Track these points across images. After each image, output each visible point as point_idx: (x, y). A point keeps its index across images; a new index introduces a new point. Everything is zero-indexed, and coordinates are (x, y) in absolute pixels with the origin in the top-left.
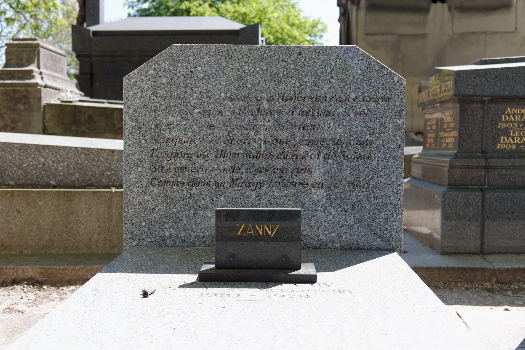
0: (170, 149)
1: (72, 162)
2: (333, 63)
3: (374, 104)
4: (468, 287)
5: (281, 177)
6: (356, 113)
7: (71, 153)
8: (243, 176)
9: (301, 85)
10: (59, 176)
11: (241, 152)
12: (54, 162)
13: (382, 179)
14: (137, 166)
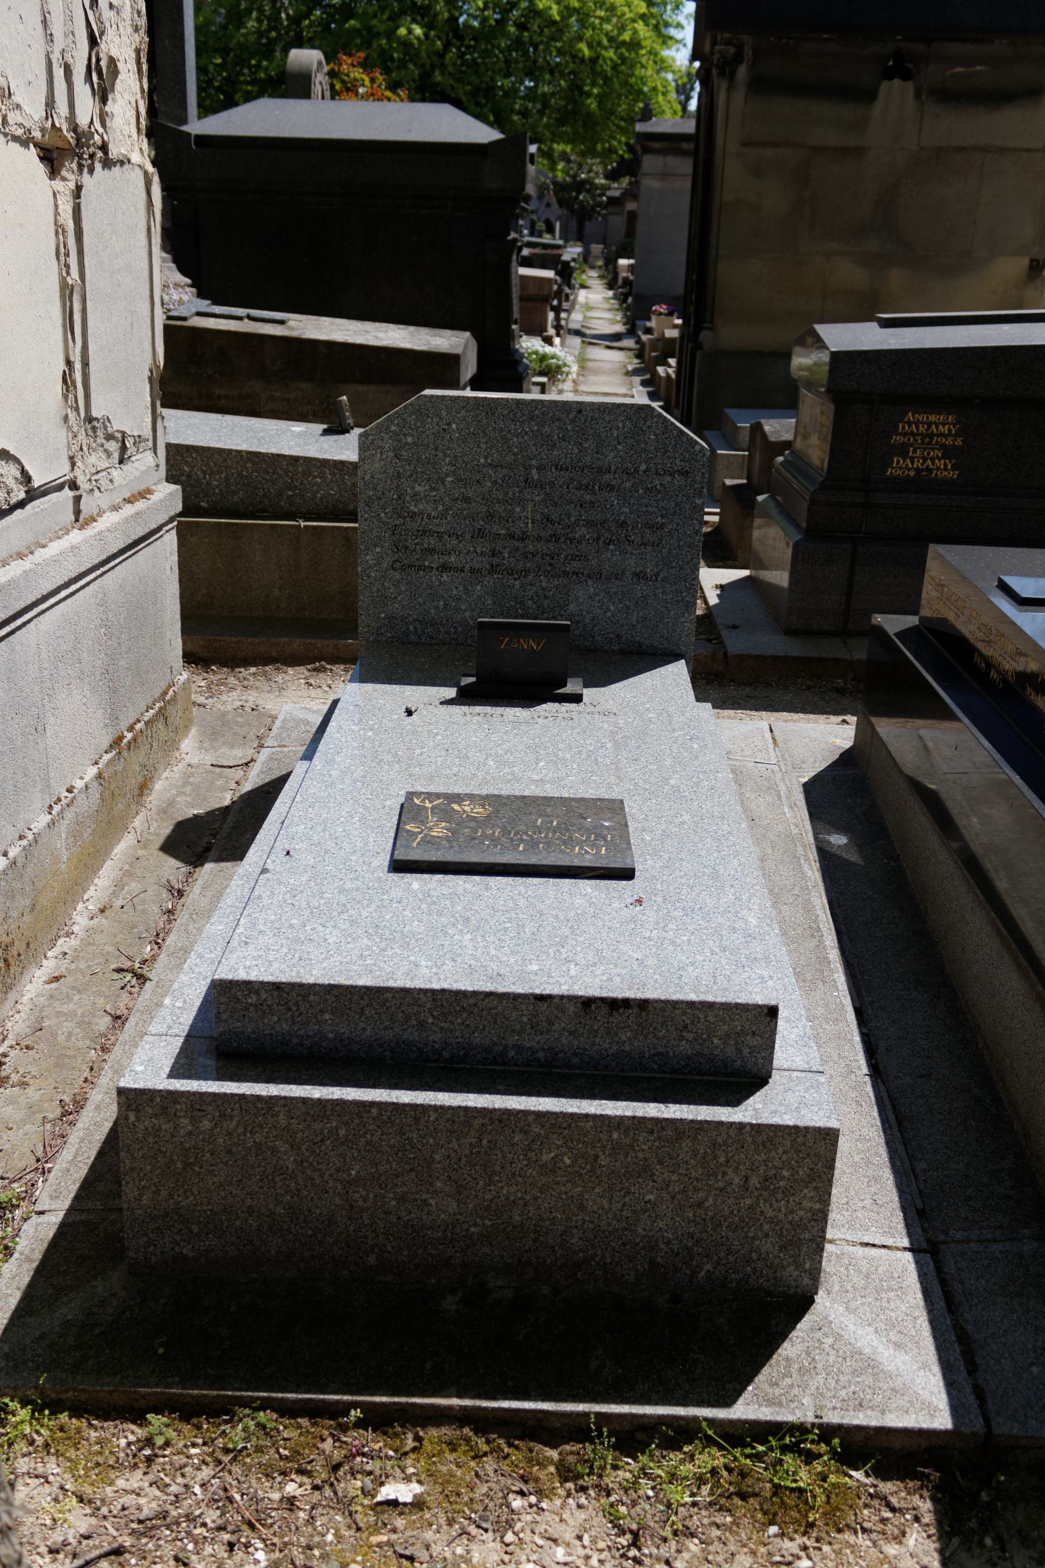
0: (415, 525)
1: (233, 474)
2: (620, 425)
3: (669, 478)
4: (811, 684)
5: (551, 565)
6: (646, 489)
7: (231, 459)
8: (505, 562)
9: (580, 451)
10: (214, 494)
11: (503, 532)
12: (204, 473)
13: (673, 571)
14: (376, 546)
